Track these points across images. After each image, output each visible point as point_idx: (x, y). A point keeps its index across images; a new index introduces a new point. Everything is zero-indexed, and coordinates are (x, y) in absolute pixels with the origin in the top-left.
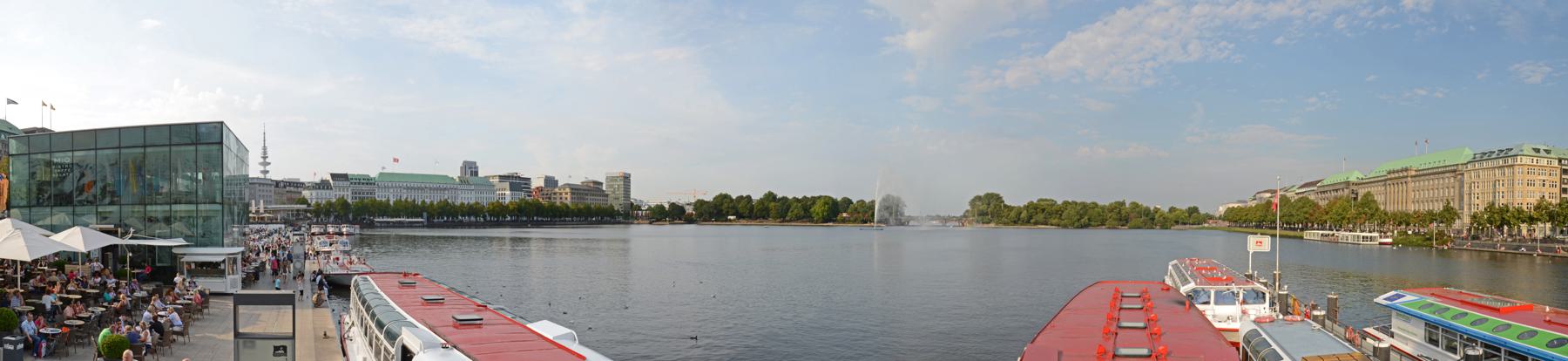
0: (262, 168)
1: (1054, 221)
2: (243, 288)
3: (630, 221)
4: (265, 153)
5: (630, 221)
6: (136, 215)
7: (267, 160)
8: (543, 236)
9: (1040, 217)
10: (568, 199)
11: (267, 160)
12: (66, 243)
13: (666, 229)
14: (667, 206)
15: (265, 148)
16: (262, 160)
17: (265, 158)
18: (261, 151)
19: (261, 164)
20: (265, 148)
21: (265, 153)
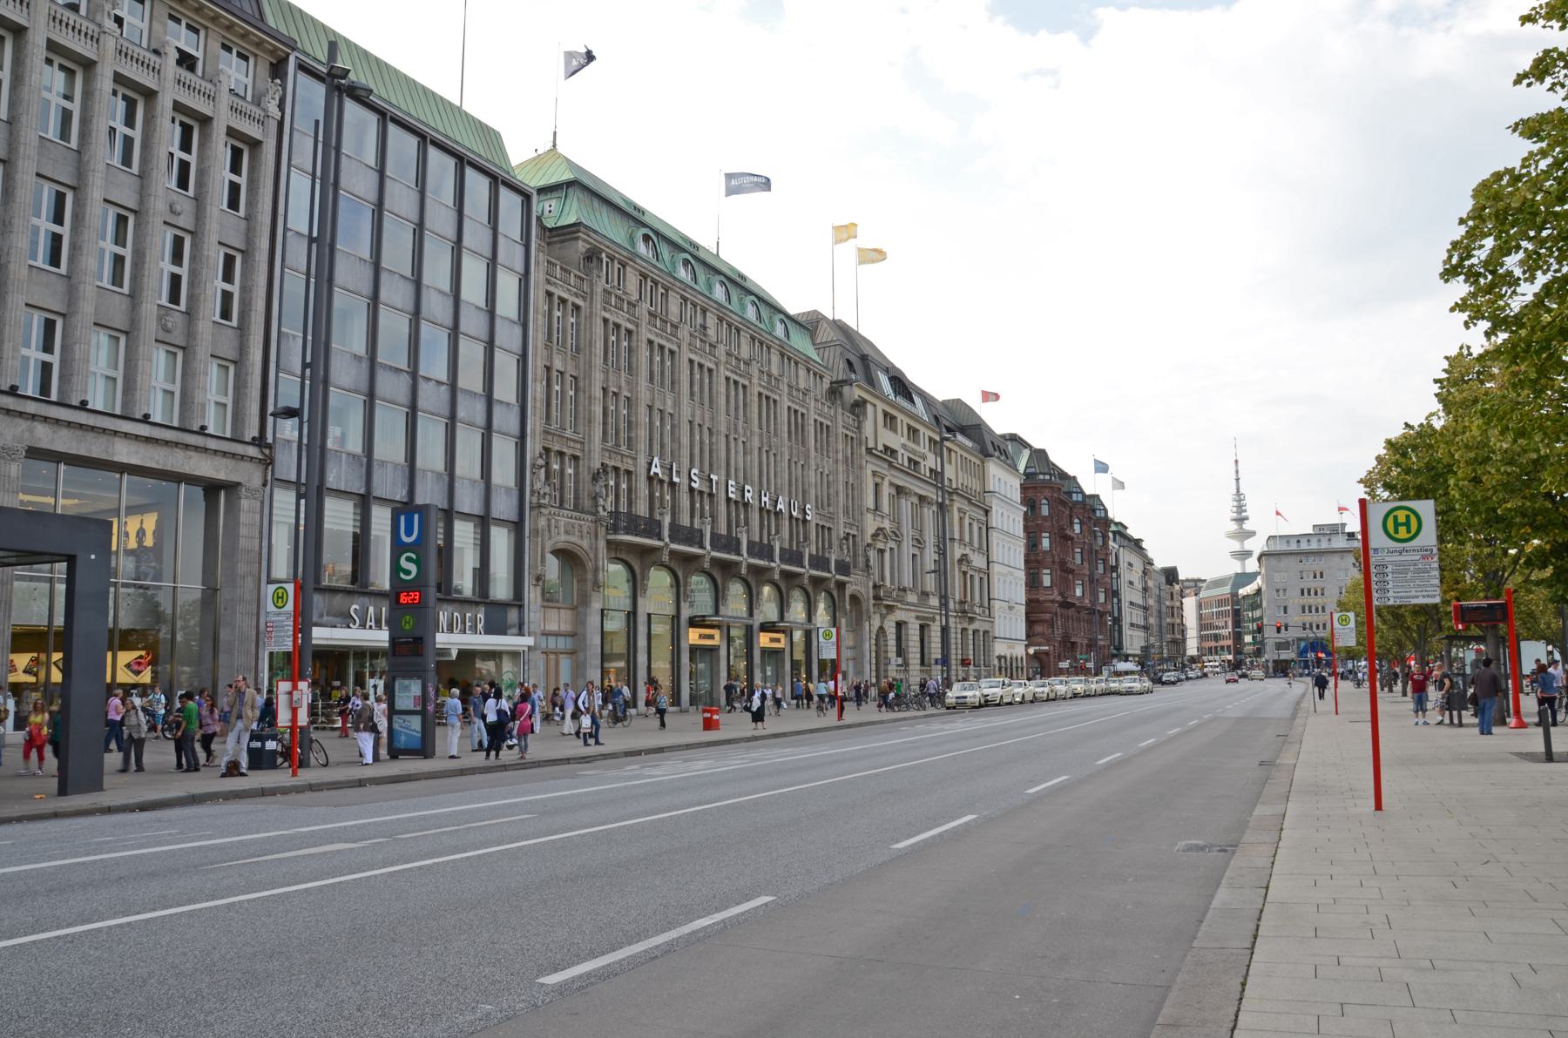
0: (1236, 546)
1: (1064, 665)
2: (836, 561)
3: (6, 250)
4: (1240, 508)
5: (6, 250)
6: (1047, 616)
7: (1247, 526)
8: (304, 32)
9: (943, 601)
10: (479, 537)
11: (1247, 526)
12: (342, 204)
13: (1247, 987)
14: (1460, 302)
15: (1239, 496)
16: (1234, 527)
17: (1241, 520)
18: (1228, 509)
19: (1233, 536)
20: (1239, 496)
21: (1240, 508)
